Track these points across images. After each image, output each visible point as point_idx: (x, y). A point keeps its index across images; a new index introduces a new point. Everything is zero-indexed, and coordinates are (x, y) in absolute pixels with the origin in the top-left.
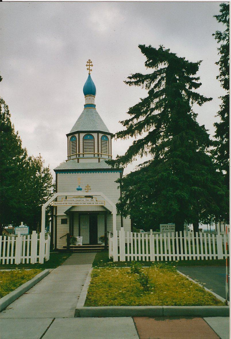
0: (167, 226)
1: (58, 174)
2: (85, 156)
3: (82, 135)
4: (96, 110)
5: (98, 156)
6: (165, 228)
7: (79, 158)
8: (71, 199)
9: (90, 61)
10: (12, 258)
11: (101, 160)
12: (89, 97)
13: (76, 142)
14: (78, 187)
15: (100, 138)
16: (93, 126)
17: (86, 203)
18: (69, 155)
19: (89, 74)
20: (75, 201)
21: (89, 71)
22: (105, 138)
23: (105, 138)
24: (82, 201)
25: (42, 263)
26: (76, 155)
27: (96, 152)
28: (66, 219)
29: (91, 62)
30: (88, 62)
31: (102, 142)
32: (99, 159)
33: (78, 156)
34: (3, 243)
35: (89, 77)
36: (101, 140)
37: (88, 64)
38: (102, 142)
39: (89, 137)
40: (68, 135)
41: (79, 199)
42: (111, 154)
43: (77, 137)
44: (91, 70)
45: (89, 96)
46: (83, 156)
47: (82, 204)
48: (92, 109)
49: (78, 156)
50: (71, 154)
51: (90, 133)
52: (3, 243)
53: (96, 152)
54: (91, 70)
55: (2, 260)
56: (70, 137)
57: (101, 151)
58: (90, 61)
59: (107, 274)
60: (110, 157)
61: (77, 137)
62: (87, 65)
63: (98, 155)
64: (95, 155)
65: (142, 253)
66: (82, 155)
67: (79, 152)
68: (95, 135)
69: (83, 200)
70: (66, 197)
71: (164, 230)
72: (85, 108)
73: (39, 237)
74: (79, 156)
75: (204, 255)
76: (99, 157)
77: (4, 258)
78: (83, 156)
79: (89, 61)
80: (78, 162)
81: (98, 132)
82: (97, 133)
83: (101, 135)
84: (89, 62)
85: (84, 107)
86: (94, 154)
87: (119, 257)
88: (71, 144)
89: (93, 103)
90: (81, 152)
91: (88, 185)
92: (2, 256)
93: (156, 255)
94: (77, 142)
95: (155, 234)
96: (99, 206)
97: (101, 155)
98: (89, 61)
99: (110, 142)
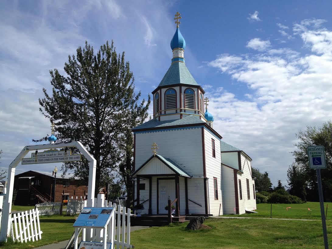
2: (167, 112)
15: (183, 91)
22: (189, 92)
23: (189, 92)
30: (176, 15)
39: (171, 92)
41: (51, 153)
51: (192, 88)
56: (155, 95)
59: (308, 230)
69: (55, 155)
82: (179, 87)
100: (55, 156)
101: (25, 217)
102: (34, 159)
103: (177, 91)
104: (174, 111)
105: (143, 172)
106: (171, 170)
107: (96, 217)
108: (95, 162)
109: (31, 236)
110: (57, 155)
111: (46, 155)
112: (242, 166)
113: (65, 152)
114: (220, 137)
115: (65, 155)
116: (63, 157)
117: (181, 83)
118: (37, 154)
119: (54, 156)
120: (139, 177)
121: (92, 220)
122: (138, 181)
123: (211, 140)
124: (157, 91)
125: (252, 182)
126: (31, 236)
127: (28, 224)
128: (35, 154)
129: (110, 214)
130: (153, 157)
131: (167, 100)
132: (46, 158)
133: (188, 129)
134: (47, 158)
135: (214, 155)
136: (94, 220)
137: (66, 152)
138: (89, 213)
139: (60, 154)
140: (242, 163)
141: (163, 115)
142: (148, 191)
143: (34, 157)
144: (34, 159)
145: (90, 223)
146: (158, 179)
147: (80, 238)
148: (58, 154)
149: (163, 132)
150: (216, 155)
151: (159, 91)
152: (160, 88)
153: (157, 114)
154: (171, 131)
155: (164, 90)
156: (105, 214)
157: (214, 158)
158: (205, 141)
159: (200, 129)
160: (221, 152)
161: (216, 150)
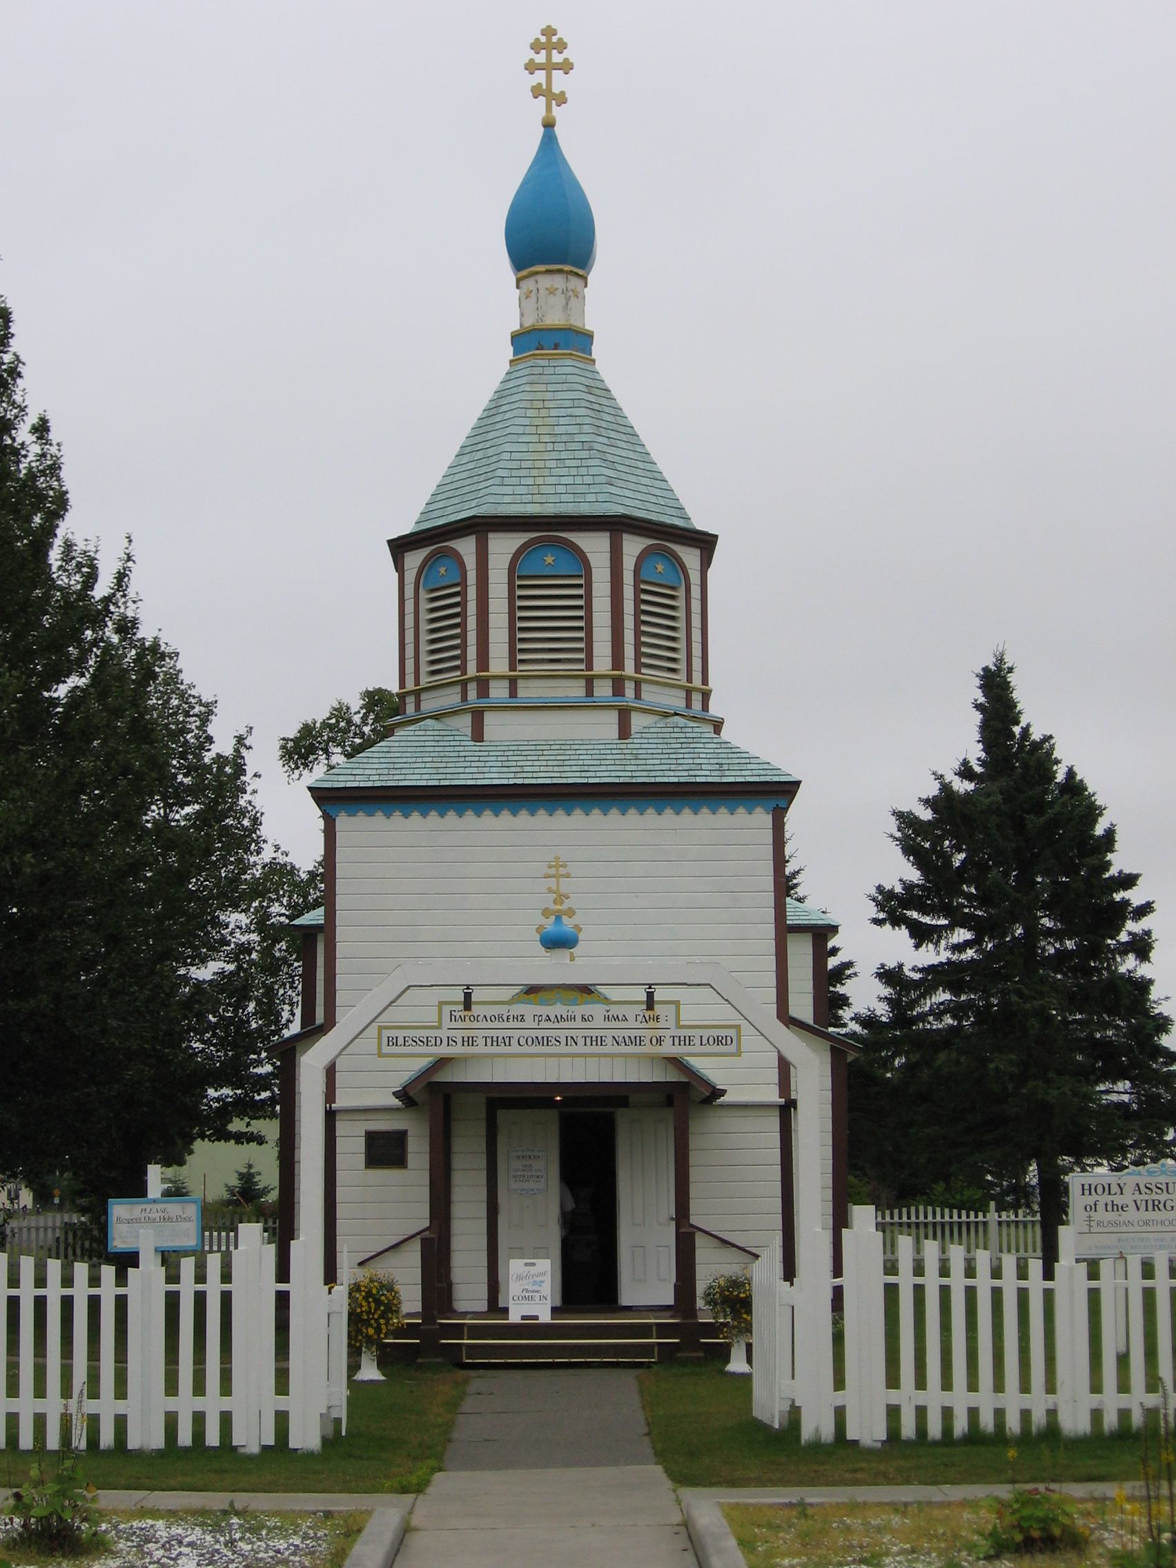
0: (1115, 1189)
1: (343, 822)
2: (528, 691)
3: (503, 547)
4: (598, 366)
5: (618, 690)
6: (1104, 1199)
7: (483, 703)
8: (502, 1010)
9: (554, 39)
10: (212, 1404)
11: (638, 722)
12: (545, 282)
13: (463, 594)
14: (549, 924)
15: (629, 563)
16: (578, 480)
17: (609, 1041)
18: (410, 686)
19: (549, 125)
20: (529, 1022)
21: (549, 108)
23: (660, 568)
24: (579, 1023)
25: (154, 1447)
26: (464, 684)
27: (602, 663)
28: (399, 1138)
29: (562, 46)
30: (536, 47)
31: (644, 597)
32: (624, 716)
33: (472, 694)
34: (14, 1303)
36: (637, 580)
37: (541, 58)
38: (644, 597)
39: (442, 570)
40: (399, 547)
42: (705, 680)
43: (470, 562)
44: (561, 99)
45: (548, 272)
46: (513, 693)
47: (581, 1041)
48: (567, 367)
49: (472, 694)
50: (425, 680)
52: (14, 1303)
53: (602, 663)
54: (561, 99)
55: (13, 1420)
56: (414, 560)
57: (638, 655)
58: (554, 39)
60: (697, 699)
61: (470, 562)
62: (532, 60)
63: (618, 685)
64: (596, 683)
65: (947, 1385)
66: (506, 683)
67: (483, 662)
68: (595, 546)
70: (468, 996)
71: (1100, 1215)
72: (515, 354)
73: (283, 1273)
74: (483, 692)
75: (973, 1399)
76: (618, 701)
77: (26, 1405)
78: (513, 693)
79: (543, 39)
80: (478, 735)
81: (617, 526)
83: (633, 546)
84: (549, 41)
85: (508, 352)
86: (590, 682)
87: (840, 1413)
88: (424, 606)
89: (575, 322)
90: (499, 663)
92: (13, 1389)
93: (894, 1397)
94: (472, 593)
95: (917, 1225)
96: (658, 1057)
97: (638, 684)
98: (543, 39)
99: (696, 592)
100: (588, 1025)
102: (458, 1035)
109: (44, 1415)
116: (633, 1033)
118: (476, 1010)
126: (44, 1415)
128: (462, 1007)
132: (534, 1033)
134: (540, 1034)
144: (458, 1035)
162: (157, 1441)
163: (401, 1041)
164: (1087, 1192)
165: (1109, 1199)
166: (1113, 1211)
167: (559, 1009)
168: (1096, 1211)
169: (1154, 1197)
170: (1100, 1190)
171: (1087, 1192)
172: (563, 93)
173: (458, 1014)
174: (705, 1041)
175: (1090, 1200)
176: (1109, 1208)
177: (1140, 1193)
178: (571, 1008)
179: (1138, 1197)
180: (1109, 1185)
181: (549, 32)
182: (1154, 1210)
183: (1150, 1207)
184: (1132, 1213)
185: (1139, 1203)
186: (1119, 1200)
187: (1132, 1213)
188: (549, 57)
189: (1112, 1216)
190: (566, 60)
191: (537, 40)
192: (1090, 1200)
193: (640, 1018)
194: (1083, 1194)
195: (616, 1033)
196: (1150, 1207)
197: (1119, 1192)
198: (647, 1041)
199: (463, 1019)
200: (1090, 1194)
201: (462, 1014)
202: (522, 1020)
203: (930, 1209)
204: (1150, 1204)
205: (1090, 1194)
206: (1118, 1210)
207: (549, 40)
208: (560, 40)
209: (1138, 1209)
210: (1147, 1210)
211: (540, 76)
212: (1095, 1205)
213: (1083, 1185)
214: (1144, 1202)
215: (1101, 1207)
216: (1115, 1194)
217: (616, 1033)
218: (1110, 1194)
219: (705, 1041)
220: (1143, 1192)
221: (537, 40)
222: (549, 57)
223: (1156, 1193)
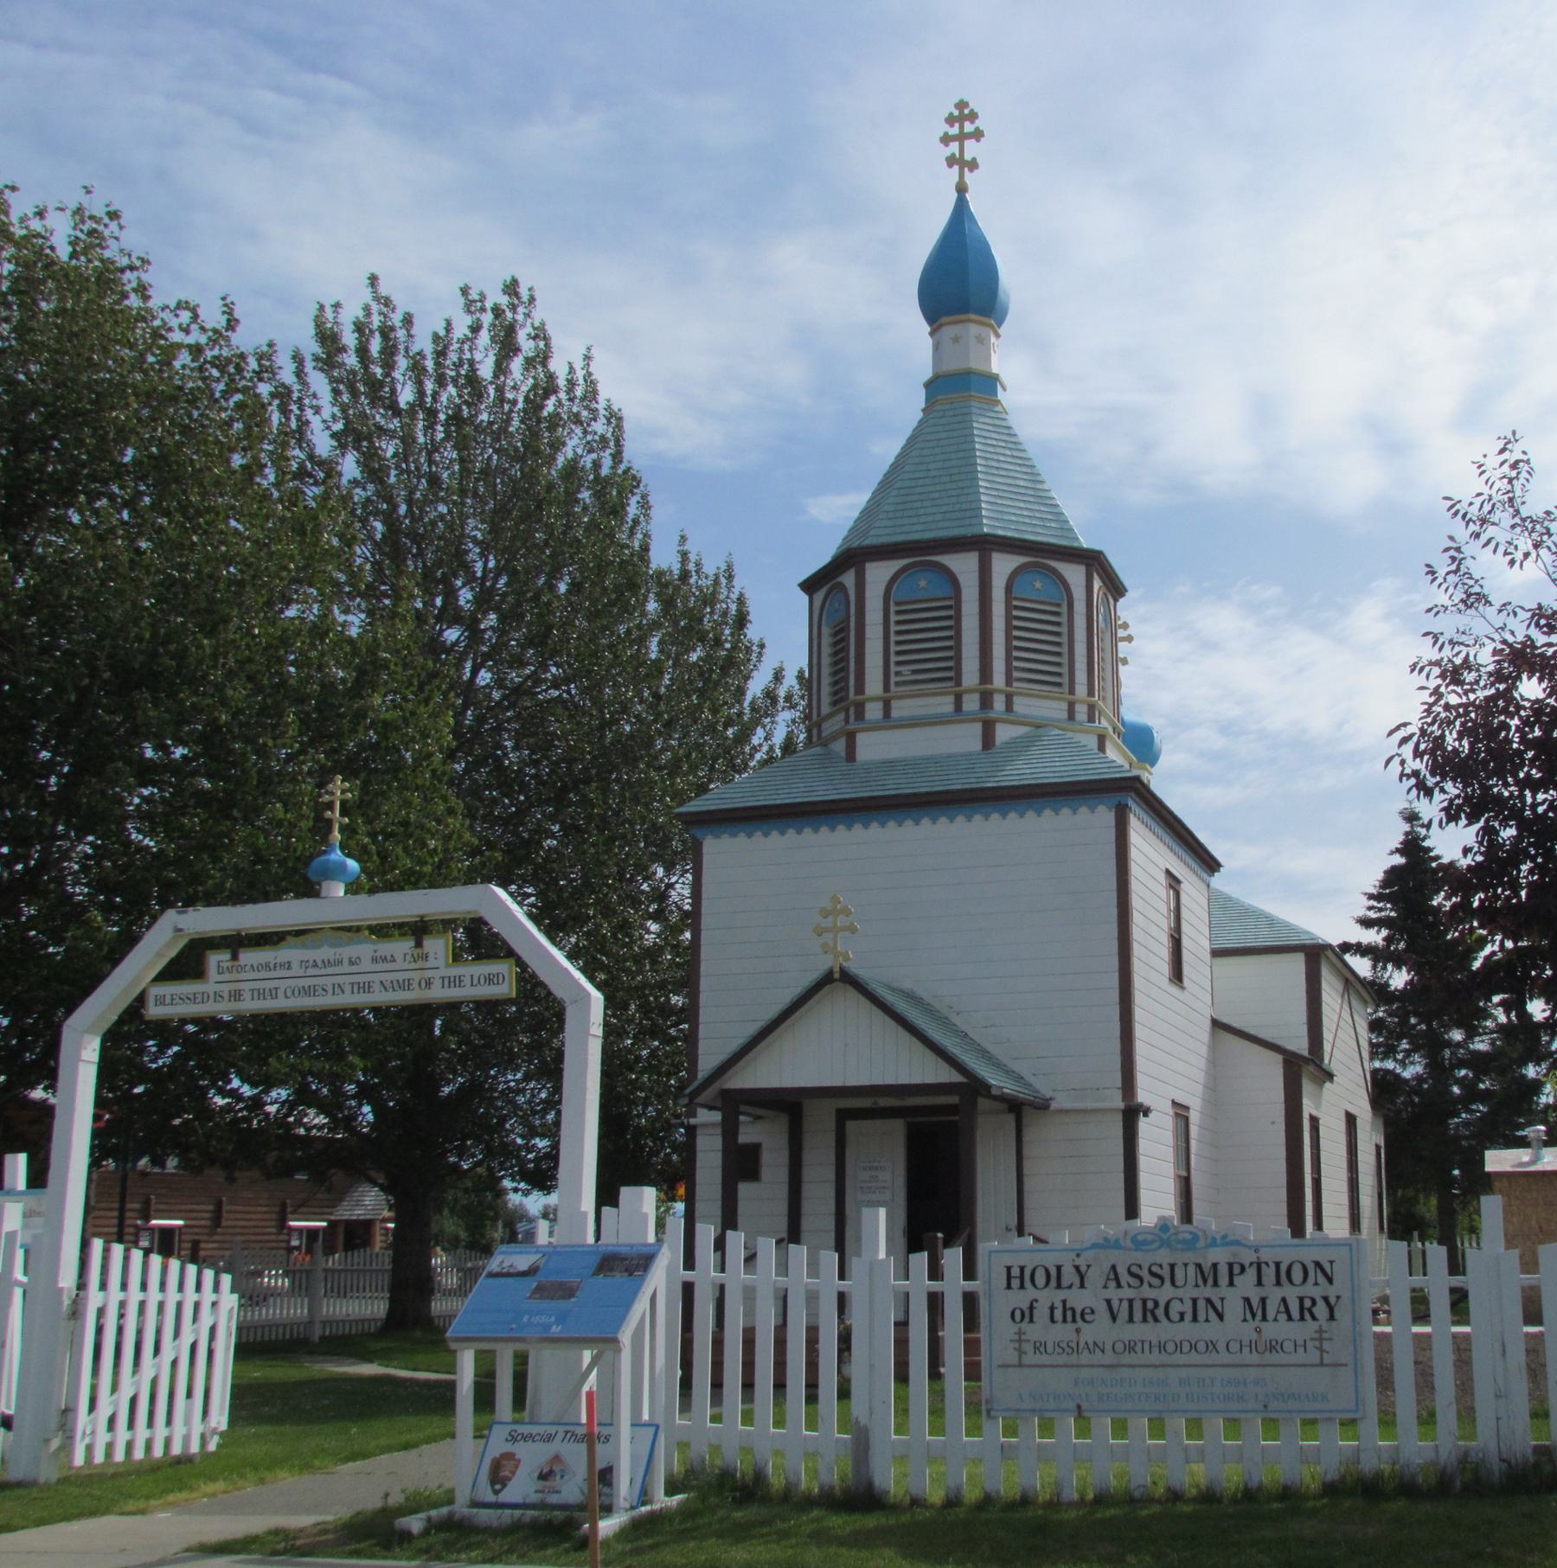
2: (900, 709)
6: (1047, 1297)
17: (377, 987)
19: (961, 189)
20: (296, 970)
22: (1038, 585)
23: (1038, 585)
29: (973, 117)
30: (950, 120)
35: (961, 208)
44: (973, 165)
47: (348, 989)
54: (973, 165)
56: (819, 596)
58: (966, 112)
62: (946, 134)
67: (860, 688)
69: (352, 963)
78: (887, 712)
83: (1003, 565)
84: (963, 114)
89: (975, 364)
90: (874, 685)
91: (835, 900)
98: (956, 113)
100: (355, 969)
101: (161, 1305)
102: (225, 988)
103: (962, 579)
104: (945, 705)
105: (764, 1074)
106: (930, 1056)
107: (566, 1291)
108: (597, 997)
110: (366, 965)
111: (295, 965)
112: (1327, 1035)
113: (412, 943)
114: (1210, 864)
115: (413, 966)
116: (401, 976)
117: (985, 530)
119: (346, 968)
120: (735, 1104)
121: (546, 1304)
122: (729, 1130)
123: (1162, 878)
124: (841, 573)
125: (1370, 1138)
127: (148, 1370)
129: (643, 1278)
130: (827, 980)
131: (898, 633)
133: (995, 816)
135: (1177, 975)
136: (563, 1305)
137: (419, 944)
138: (532, 1271)
139: (384, 959)
140: (1325, 1019)
141: (875, 727)
142: (782, 1191)
143: (227, 977)
144: (225, 988)
145: (536, 1319)
146: (843, 1116)
147: (719, 1253)
148: (374, 960)
149: (858, 828)
150: (1186, 970)
151: (848, 579)
152: (851, 558)
153: (831, 715)
154: (977, 818)
155: (878, 574)
156: (619, 1279)
157: (1174, 990)
158: (1135, 886)
159: (1104, 817)
160: (632, 1425)
161: (1185, 942)
162: (1076, 1496)
163: (168, 1000)
164: (1015, 1283)
165: (1057, 1297)
166: (1065, 1320)
167: (326, 953)
168: (1031, 1321)
169: (1147, 1292)
170: (1040, 1278)
171: (1015, 1283)
172: (974, 160)
173: (224, 965)
174: (475, 982)
175: (1021, 1299)
176: (1058, 1314)
177: (1119, 1286)
178: (339, 950)
179: (1113, 1293)
180: (1059, 1268)
181: (961, 105)
182: (1145, 1320)
183: (1138, 1315)
184: (1099, 1329)
185: (1115, 1304)
186: (1079, 1299)
187: (1099, 1329)
188: (961, 128)
189: (1063, 1332)
190: (977, 129)
191: (951, 114)
192: (1021, 1299)
193: (408, 958)
194: (1009, 1286)
195: (383, 977)
196: (1138, 1315)
197: (1077, 1282)
198: (415, 985)
199: (229, 970)
200: (1022, 1287)
201: (229, 964)
202: (289, 968)
203: (192, 1269)
204: (1138, 1306)
205: (1022, 1287)
206: (1074, 1321)
207: (961, 112)
208: (972, 111)
209: (1114, 1318)
210: (1131, 1320)
211: (954, 147)
212: (1031, 1308)
213: (1009, 1269)
214: (1125, 1304)
215: (1041, 1312)
216: (1070, 1287)
217: (383, 977)
218: (1059, 1286)
219: (475, 982)
220: (1123, 1283)
221: (951, 114)
222: (961, 128)
223: (1150, 1286)
